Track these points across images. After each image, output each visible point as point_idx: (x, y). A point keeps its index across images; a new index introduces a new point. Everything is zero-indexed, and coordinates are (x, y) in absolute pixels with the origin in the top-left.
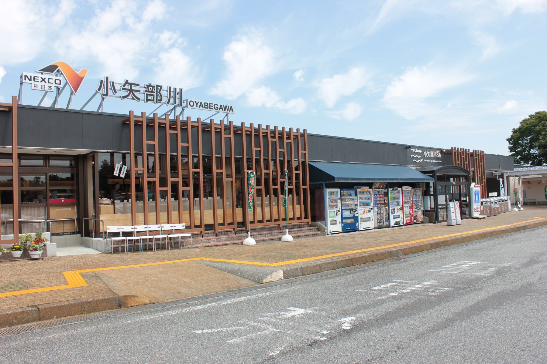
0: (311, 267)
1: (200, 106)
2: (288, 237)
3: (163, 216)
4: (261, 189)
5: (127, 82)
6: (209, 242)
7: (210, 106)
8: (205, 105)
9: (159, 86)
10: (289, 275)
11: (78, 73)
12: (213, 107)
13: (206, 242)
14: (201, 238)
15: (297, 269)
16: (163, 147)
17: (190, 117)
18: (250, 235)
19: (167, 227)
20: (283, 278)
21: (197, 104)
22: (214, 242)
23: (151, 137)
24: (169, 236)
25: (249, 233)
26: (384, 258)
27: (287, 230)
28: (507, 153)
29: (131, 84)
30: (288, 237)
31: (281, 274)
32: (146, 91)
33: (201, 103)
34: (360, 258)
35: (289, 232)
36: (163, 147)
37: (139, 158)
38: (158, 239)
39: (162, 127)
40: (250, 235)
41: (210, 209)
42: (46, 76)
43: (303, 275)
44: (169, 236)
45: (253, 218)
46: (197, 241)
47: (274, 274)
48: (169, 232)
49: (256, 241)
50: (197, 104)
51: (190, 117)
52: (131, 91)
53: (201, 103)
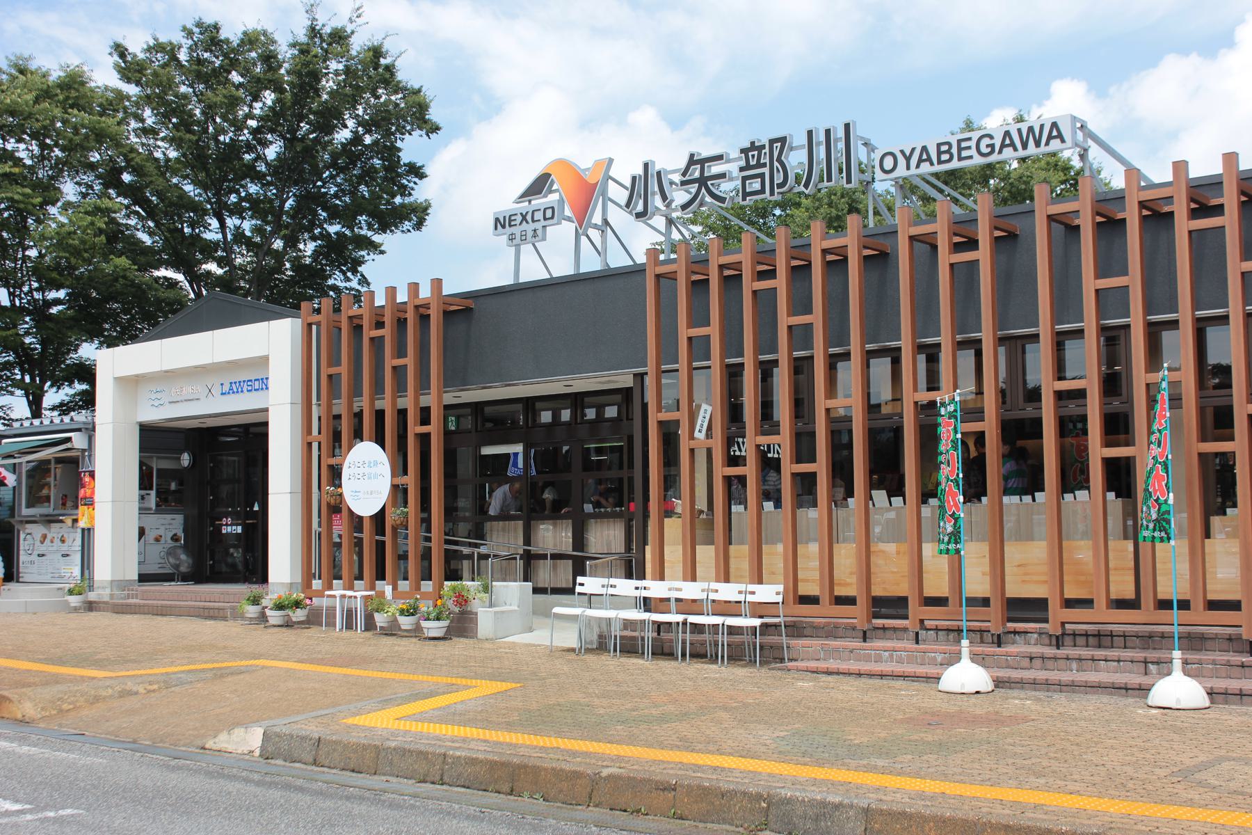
0: (346, 746)
1: (920, 161)
2: (966, 675)
3: (740, 553)
4: (814, 475)
5: (692, 161)
6: (879, 660)
7: (960, 149)
8: (939, 153)
9: (776, 140)
10: (273, 748)
11: (586, 178)
12: (973, 152)
13: (867, 659)
14: (910, 645)
15: (303, 738)
16: (732, 342)
17: (1185, 163)
18: (1177, 664)
19: (691, 591)
20: (257, 753)
21: (908, 159)
22: (900, 661)
23: (699, 317)
24: (692, 619)
25: (965, 643)
26: (590, 800)
27: (1177, 654)
28: (444, 293)
29: (703, 162)
30: (1178, 689)
31: (252, 739)
32: (742, 169)
33: (924, 149)
34: (403, 752)
35: (1185, 662)
36: (732, 342)
37: (699, 377)
38: (732, 630)
39: (1157, 217)
40: (1177, 664)
41: (983, 540)
42: (538, 202)
43: (315, 763)
44: (692, 619)
45: (1132, 587)
46: (836, 650)
47: (239, 732)
48: (691, 606)
49: (1210, 693)
50: (908, 159)
51: (1185, 163)
52: (702, 181)
53: (924, 149)
